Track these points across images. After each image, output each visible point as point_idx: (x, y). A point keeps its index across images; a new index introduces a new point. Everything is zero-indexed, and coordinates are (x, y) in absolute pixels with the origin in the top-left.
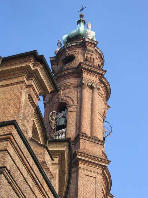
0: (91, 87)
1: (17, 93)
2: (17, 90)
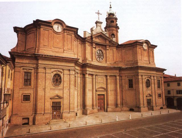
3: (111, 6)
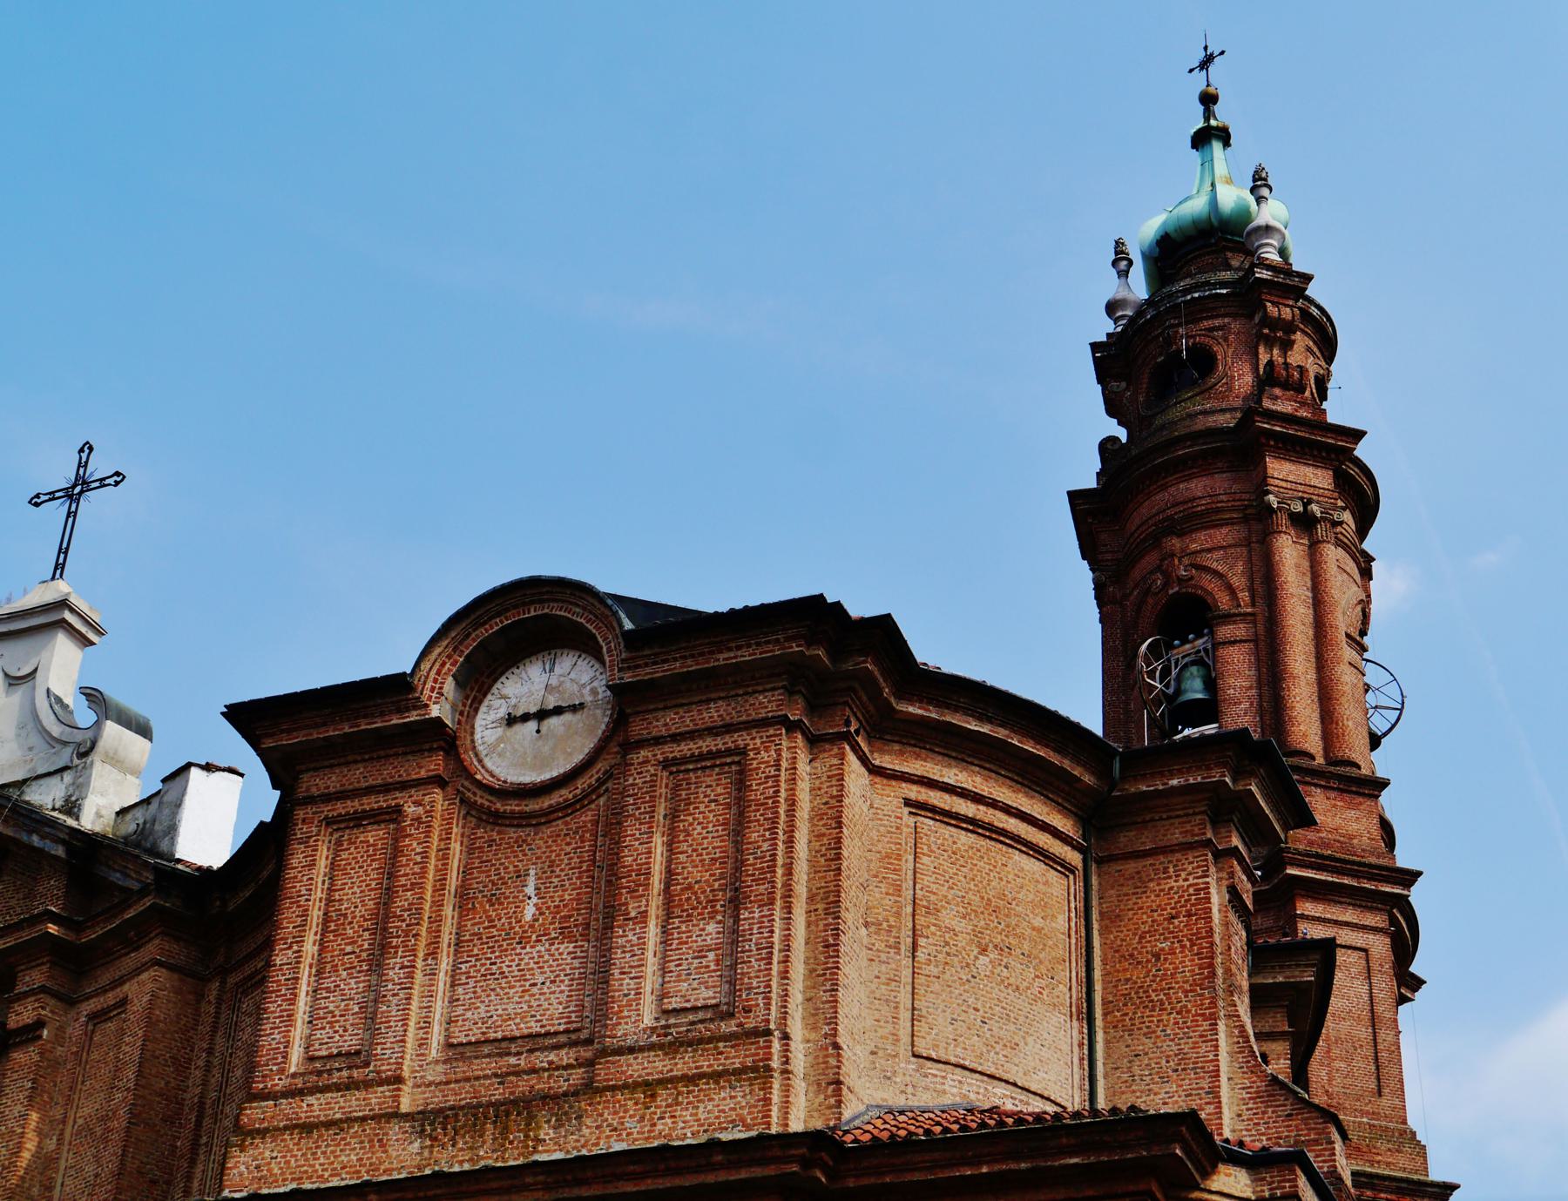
0: (1305, 523)
1: (1191, 891)
2: (1191, 878)
3: (1223, 114)
